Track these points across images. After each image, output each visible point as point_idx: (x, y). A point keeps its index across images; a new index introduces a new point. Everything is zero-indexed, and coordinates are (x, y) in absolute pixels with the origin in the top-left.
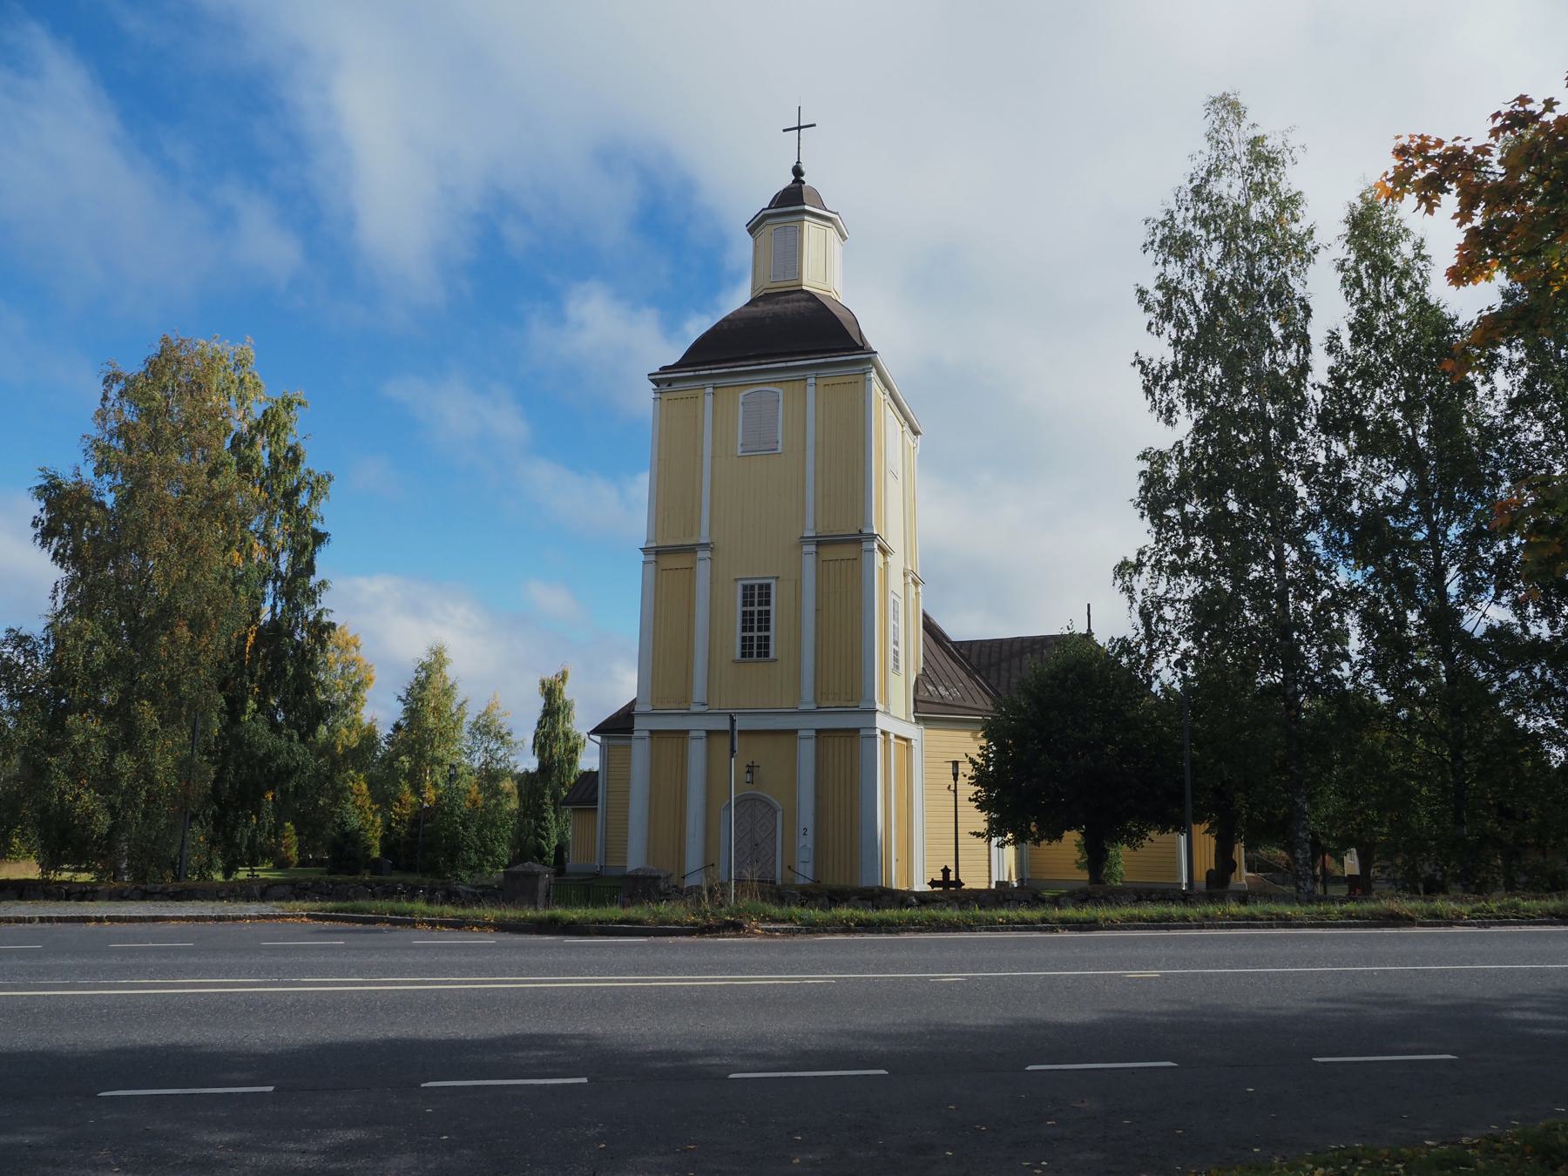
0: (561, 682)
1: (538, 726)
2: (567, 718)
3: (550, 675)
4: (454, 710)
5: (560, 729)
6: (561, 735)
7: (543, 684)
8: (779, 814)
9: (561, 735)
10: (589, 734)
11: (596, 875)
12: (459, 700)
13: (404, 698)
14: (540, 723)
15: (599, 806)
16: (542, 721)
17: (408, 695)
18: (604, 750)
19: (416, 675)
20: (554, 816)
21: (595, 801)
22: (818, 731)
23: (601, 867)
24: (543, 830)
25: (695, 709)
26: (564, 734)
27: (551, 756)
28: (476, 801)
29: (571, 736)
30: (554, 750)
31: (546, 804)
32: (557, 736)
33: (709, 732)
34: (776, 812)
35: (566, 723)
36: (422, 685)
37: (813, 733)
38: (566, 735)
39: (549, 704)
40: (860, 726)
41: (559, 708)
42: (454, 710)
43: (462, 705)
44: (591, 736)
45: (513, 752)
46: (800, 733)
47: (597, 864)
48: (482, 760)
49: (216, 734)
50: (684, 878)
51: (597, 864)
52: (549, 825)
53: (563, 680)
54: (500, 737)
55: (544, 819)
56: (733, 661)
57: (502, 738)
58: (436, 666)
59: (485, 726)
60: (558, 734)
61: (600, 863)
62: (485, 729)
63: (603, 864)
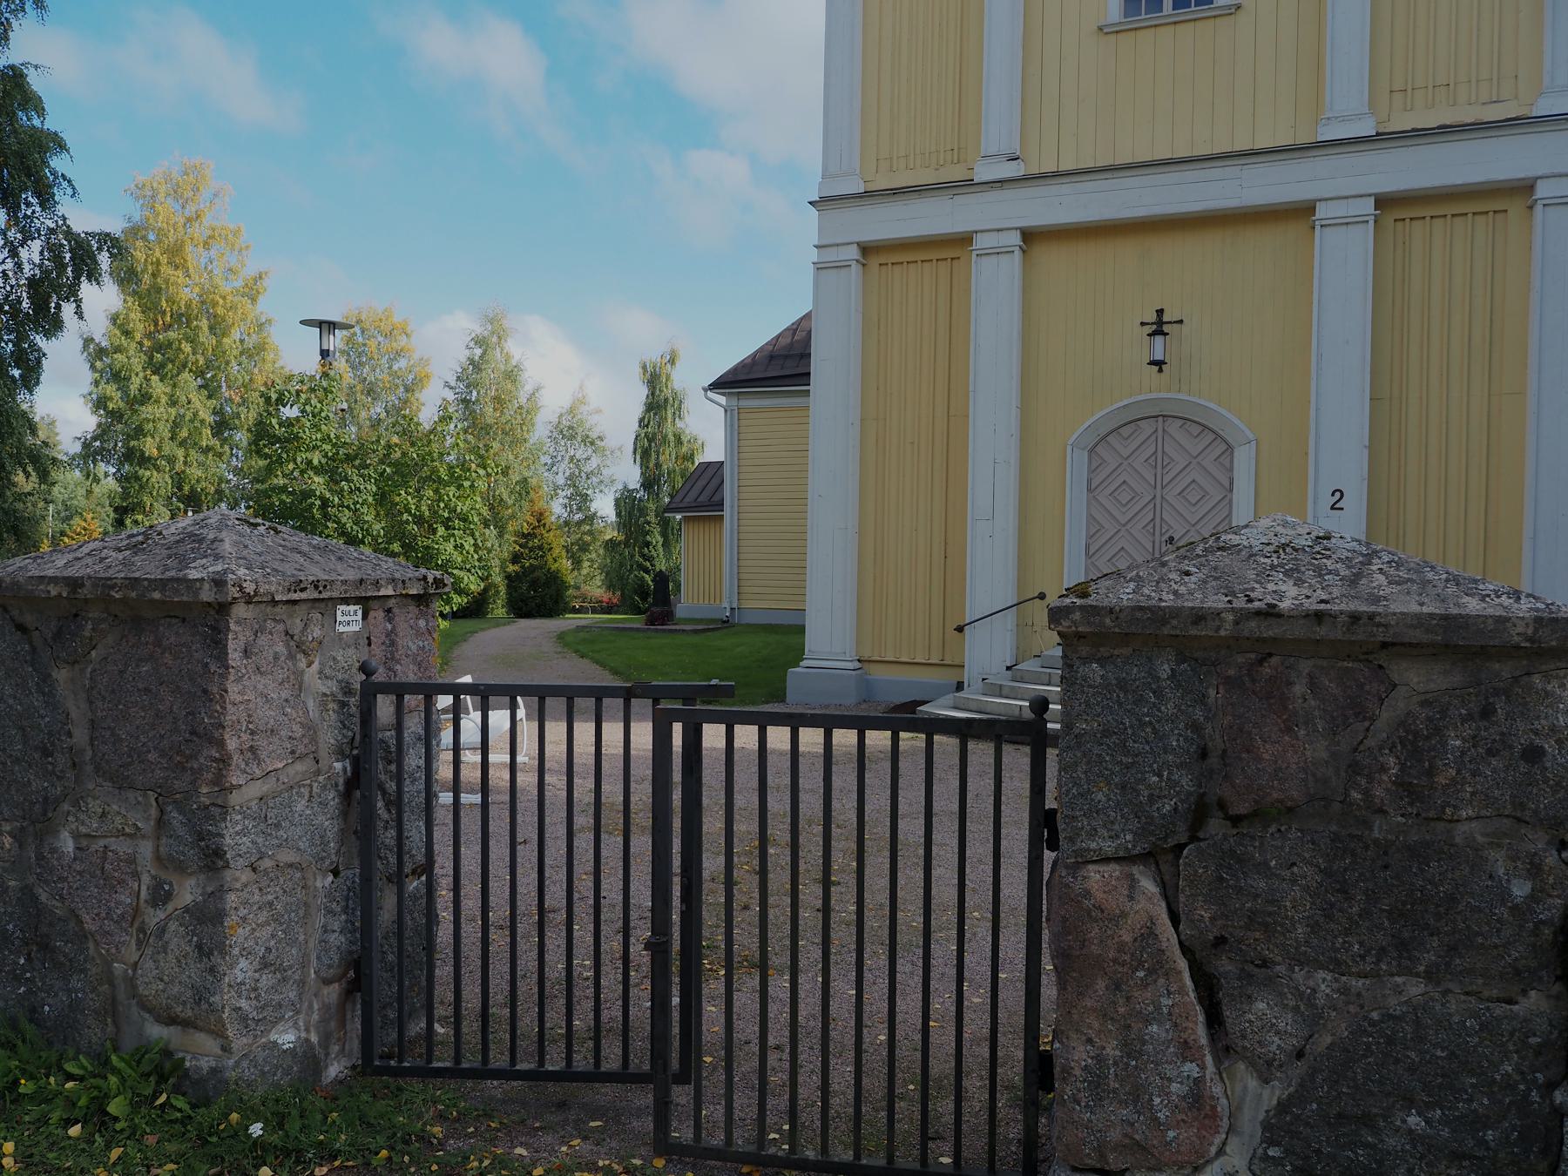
0: (669, 366)
1: (640, 426)
2: (678, 413)
3: (654, 355)
4: (523, 400)
5: (669, 429)
6: (671, 438)
7: (644, 368)
8: (1244, 461)
9: (671, 438)
10: (705, 390)
11: (724, 622)
12: (529, 388)
13: (453, 384)
14: (641, 420)
15: (727, 513)
16: (644, 417)
17: (458, 379)
18: (732, 418)
19: (467, 353)
20: (661, 540)
21: (720, 505)
22: (1384, 202)
23: (732, 609)
24: (645, 560)
25: (983, 173)
26: (675, 435)
27: (658, 465)
28: (541, 514)
29: (685, 439)
30: (662, 458)
31: (649, 523)
32: (665, 437)
33: (1029, 236)
34: (1230, 449)
35: (677, 419)
36: (476, 365)
37: (1368, 206)
38: (679, 440)
39: (653, 394)
40: (1531, 174)
41: (666, 400)
42: (523, 400)
43: (534, 394)
44: (709, 393)
45: (608, 463)
46: (1322, 211)
47: (726, 604)
48: (567, 474)
49: (1359, 797)
50: (960, 629)
51: (726, 604)
52: (653, 553)
53: (672, 361)
54: (589, 441)
55: (648, 544)
56: (1100, 29)
57: (592, 443)
58: (495, 339)
59: (571, 428)
60: (666, 436)
61: (731, 602)
62: (570, 431)
63: (735, 606)
